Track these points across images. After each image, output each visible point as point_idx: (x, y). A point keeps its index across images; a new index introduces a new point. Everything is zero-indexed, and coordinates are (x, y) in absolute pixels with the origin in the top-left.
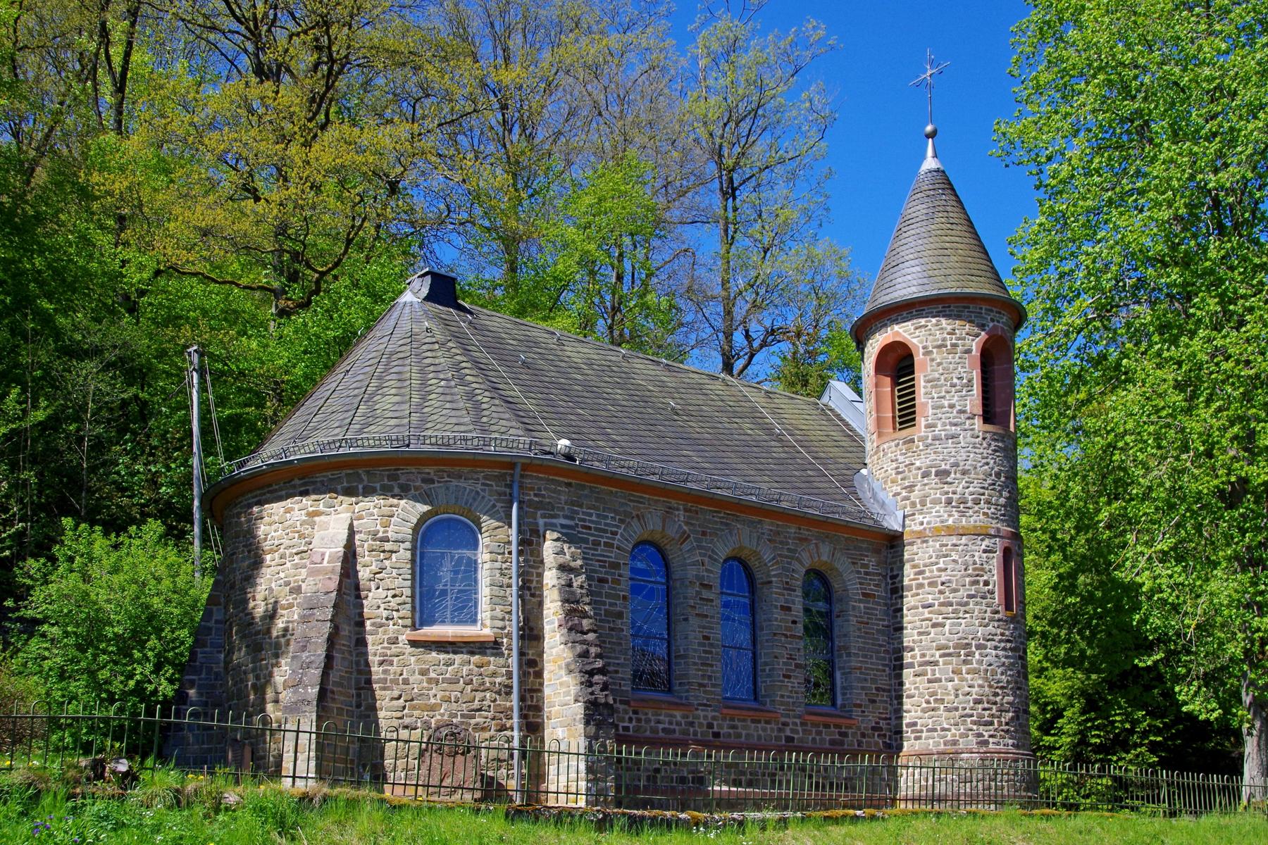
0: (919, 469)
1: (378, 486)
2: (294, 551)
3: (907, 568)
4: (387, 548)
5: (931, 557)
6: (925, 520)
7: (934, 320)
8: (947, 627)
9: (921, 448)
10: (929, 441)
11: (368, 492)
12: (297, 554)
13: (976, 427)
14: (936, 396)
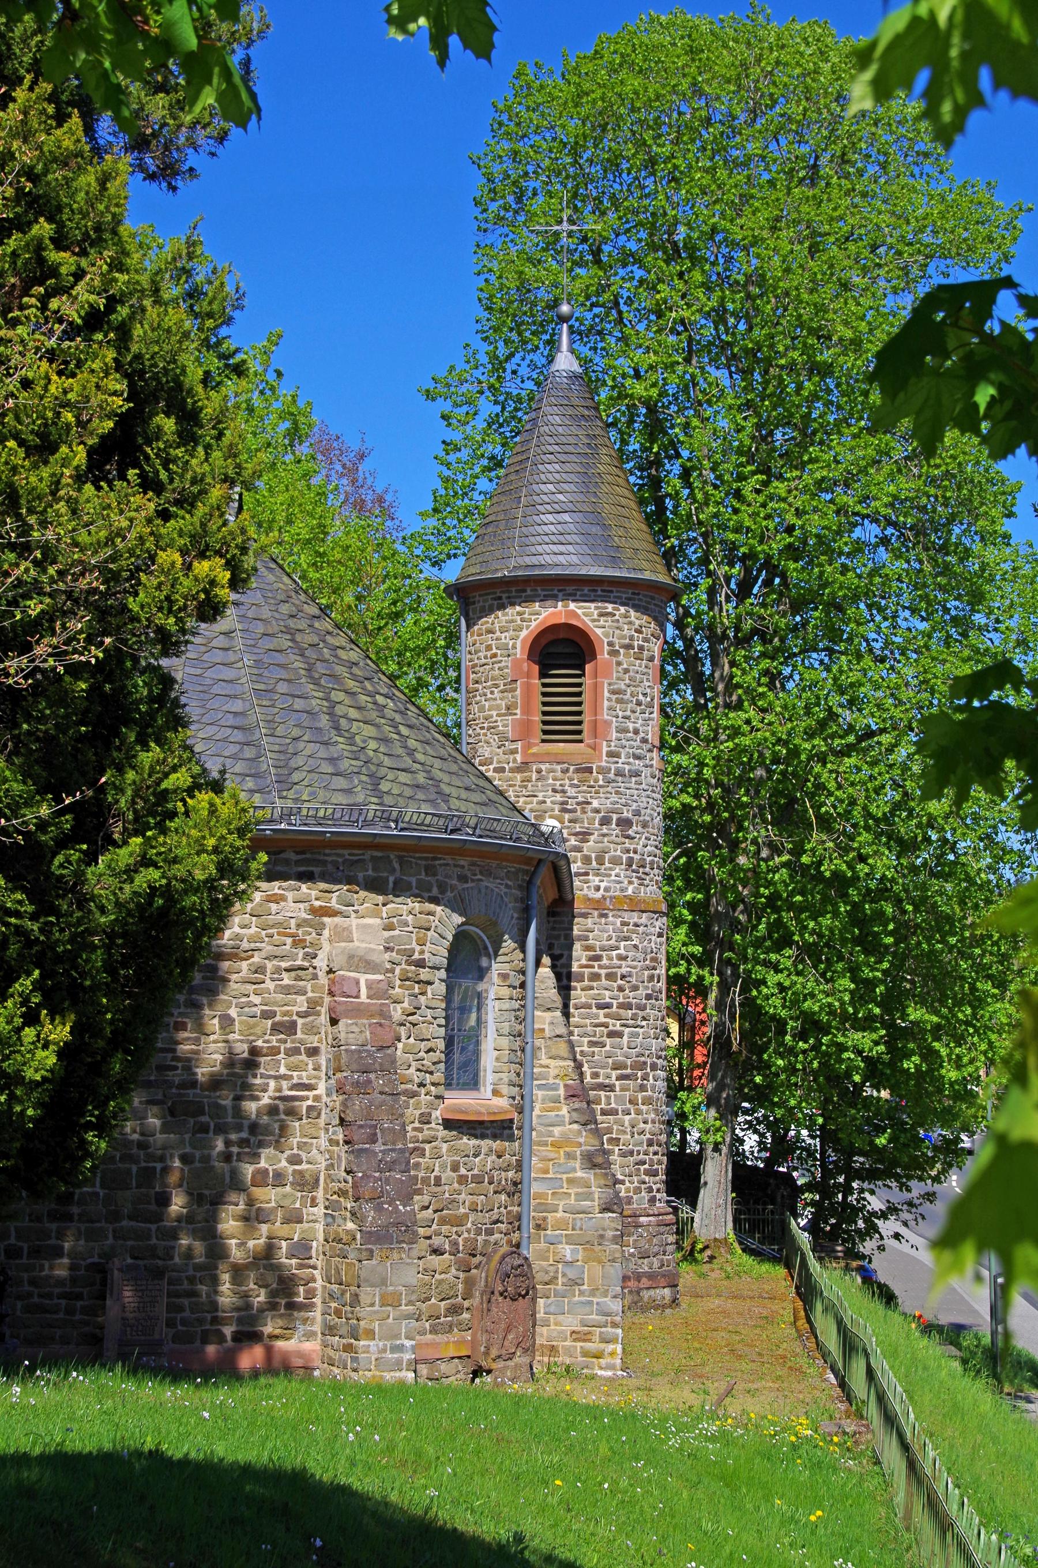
0: (597, 811)
1: (413, 880)
2: (284, 965)
3: (577, 949)
4: (422, 977)
5: (610, 938)
6: (603, 885)
7: (622, 609)
8: (625, 1038)
9: (601, 783)
10: (612, 775)
11: (400, 889)
12: (287, 970)
13: (654, 762)
14: (621, 714)
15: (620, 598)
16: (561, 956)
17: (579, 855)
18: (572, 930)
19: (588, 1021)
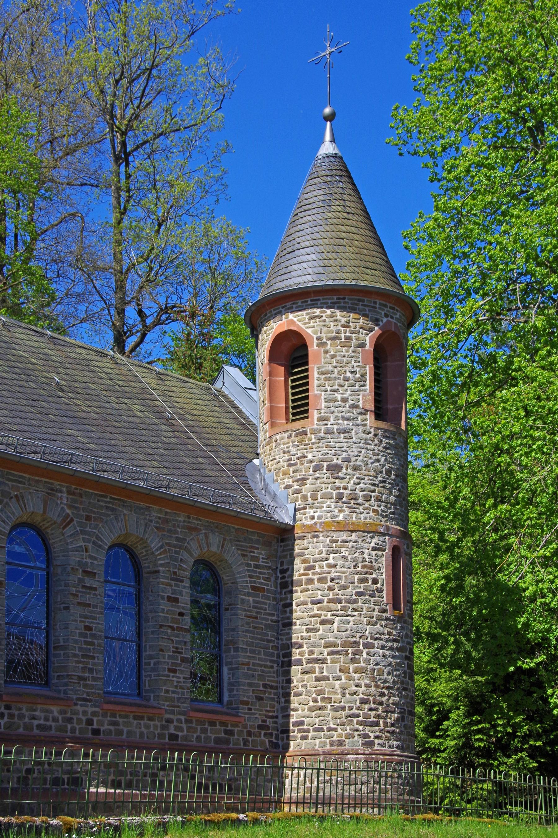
0: (311, 462)
6: (316, 515)
7: (329, 311)
8: (336, 624)
9: (314, 440)
13: (368, 422)
14: (329, 388)
15: (327, 303)
16: (287, 570)
17: (299, 495)
18: (293, 550)
19: (306, 614)
